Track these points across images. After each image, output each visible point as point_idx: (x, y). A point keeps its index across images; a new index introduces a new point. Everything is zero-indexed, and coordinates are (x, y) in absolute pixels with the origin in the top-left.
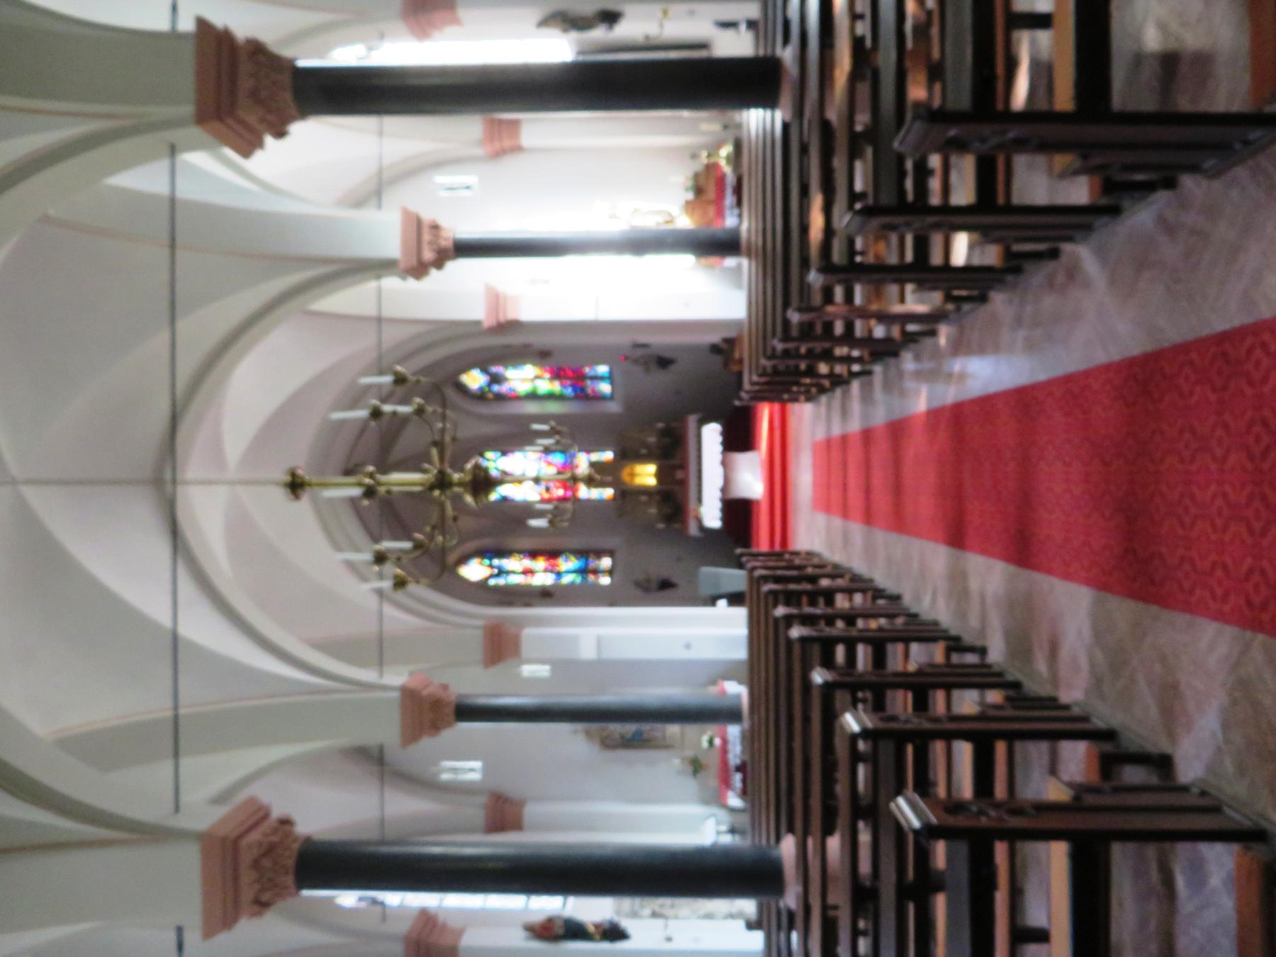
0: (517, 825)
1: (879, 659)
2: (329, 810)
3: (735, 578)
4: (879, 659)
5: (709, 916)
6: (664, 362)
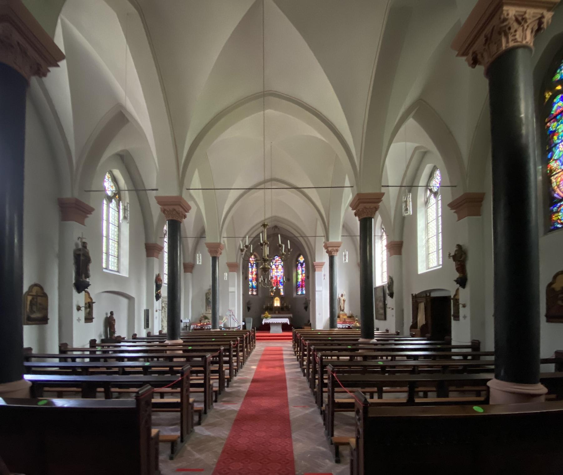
0: (185, 271)
1: (226, 362)
2: (189, 224)
3: (250, 327)
4: (226, 362)
5: (162, 321)
6: (306, 308)
